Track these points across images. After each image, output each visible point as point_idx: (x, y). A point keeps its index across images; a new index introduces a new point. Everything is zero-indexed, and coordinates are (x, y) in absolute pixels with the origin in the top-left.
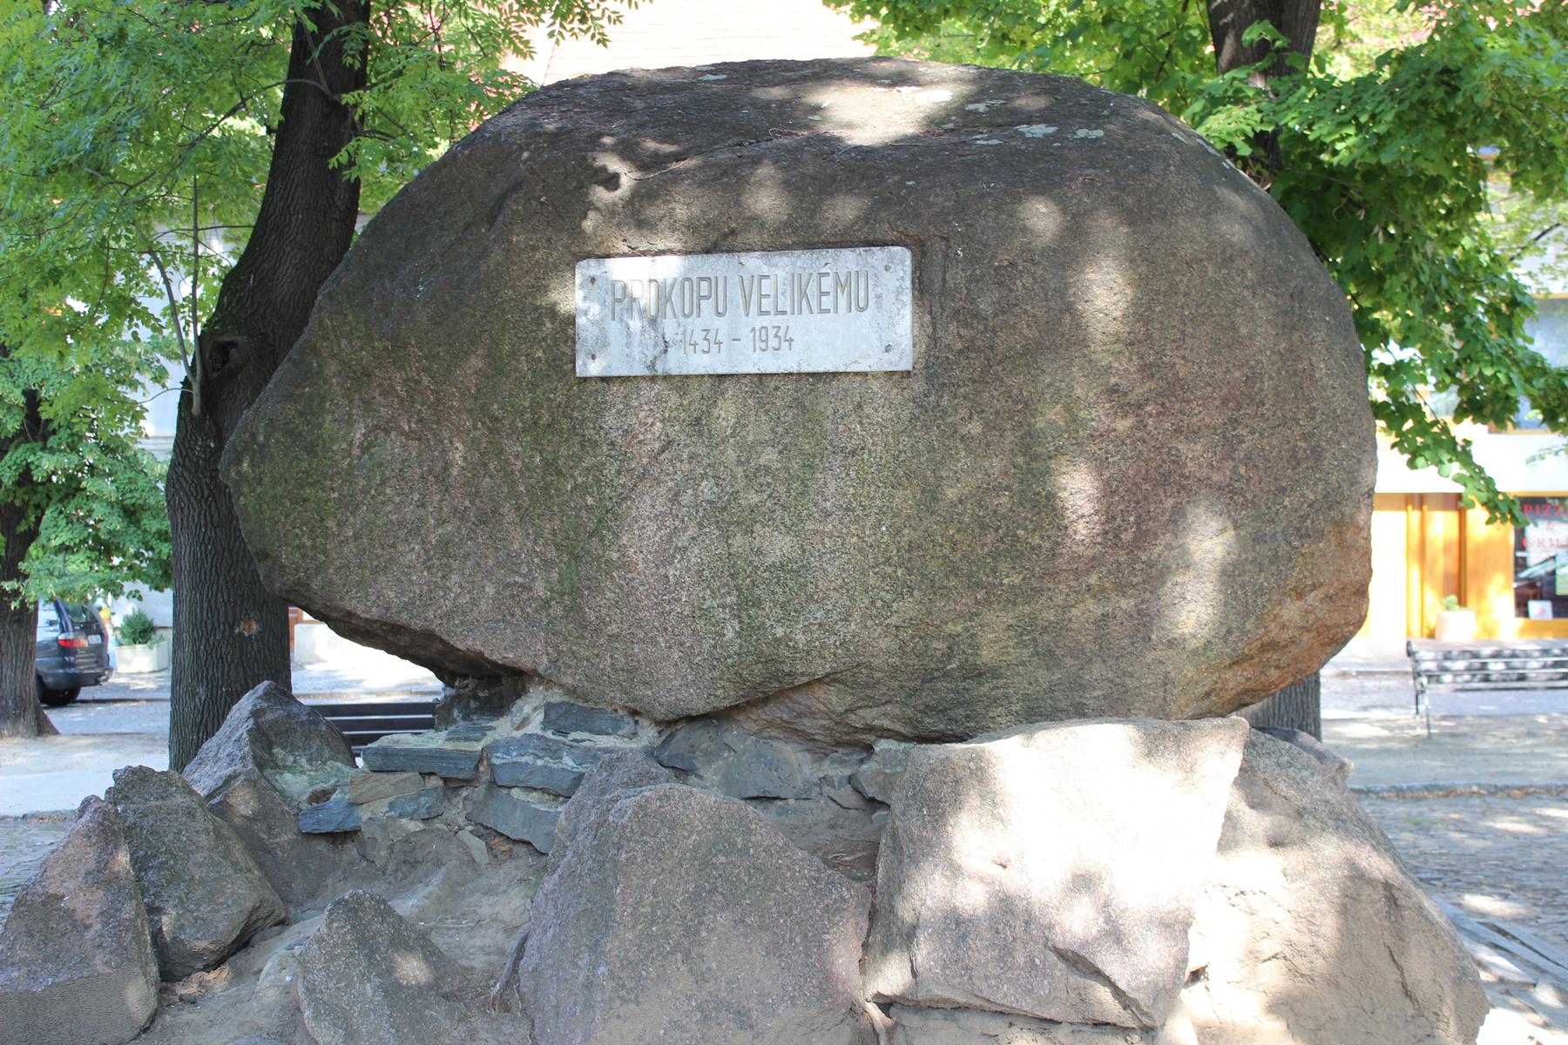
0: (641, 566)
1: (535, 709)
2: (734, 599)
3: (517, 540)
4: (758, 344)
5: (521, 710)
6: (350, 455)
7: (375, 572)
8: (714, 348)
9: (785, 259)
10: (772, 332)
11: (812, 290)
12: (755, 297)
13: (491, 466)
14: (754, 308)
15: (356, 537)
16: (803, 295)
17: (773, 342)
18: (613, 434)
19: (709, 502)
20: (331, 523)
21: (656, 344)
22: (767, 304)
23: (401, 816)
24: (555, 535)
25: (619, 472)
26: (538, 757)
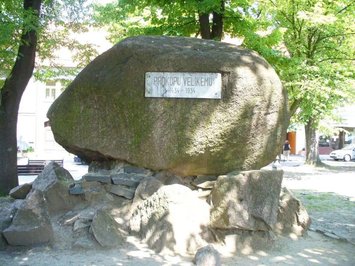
0: (156, 138)
1: (121, 168)
2: (177, 145)
3: (124, 132)
4: (187, 92)
5: (117, 168)
6: (80, 113)
7: (84, 138)
8: (193, 92)
9: (194, 74)
10: (190, 89)
11: (200, 81)
12: (187, 82)
13: (119, 116)
14: (186, 84)
15: (80, 130)
16: (198, 82)
17: (191, 91)
18: (152, 109)
19: (173, 124)
20: (74, 128)
21: (164, 91)
22: (189, 83)
23: (93, 191)
24: (135, 131)
25: (153, 118)
26: (124, 178)
